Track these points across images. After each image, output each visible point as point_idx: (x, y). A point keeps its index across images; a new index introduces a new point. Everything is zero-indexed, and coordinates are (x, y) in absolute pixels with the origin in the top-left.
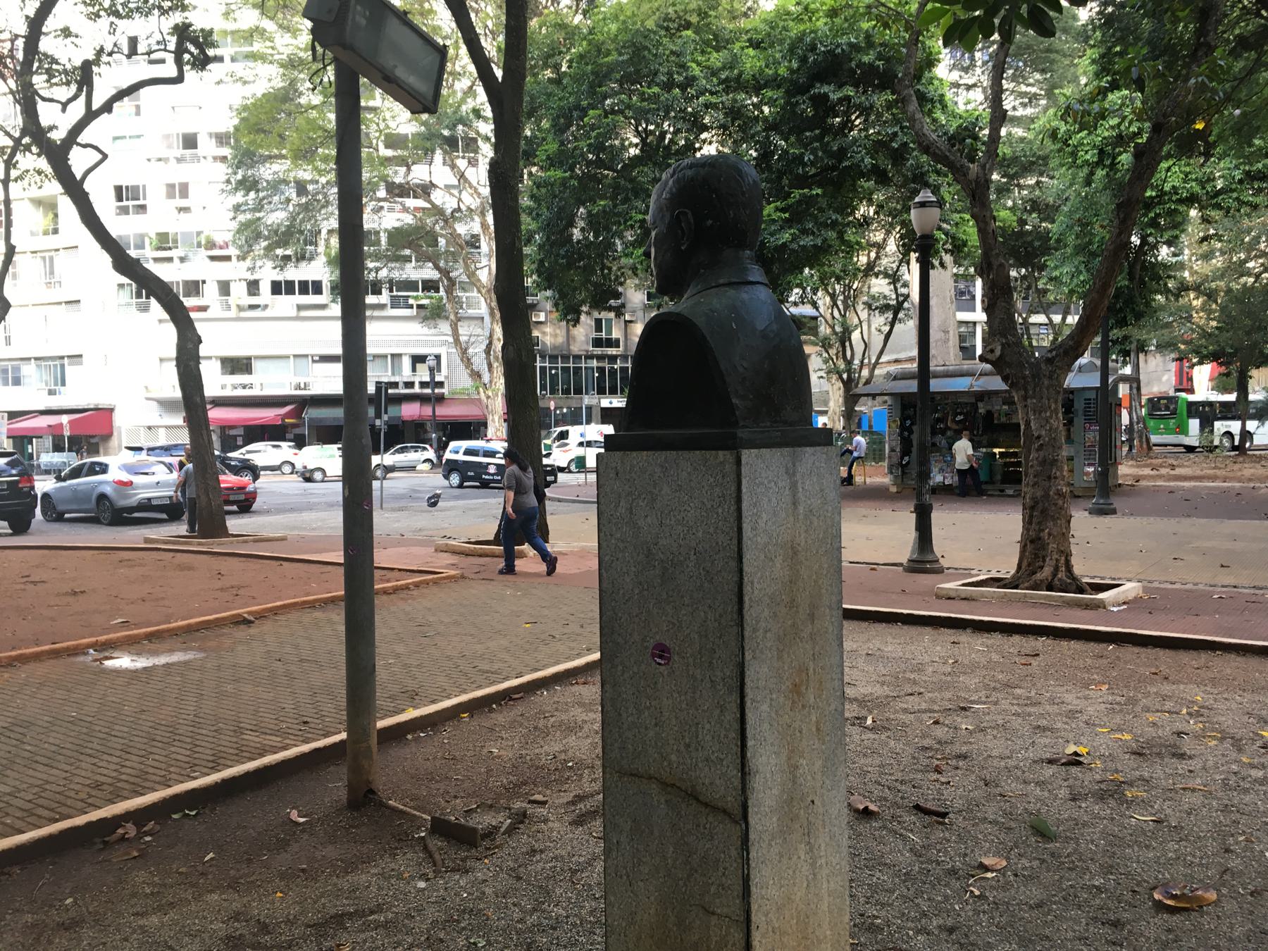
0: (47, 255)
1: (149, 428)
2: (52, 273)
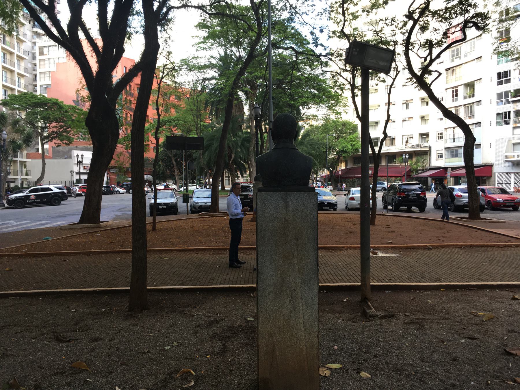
0: (469, 105)
1: (507, 173)
2: (471, 112)
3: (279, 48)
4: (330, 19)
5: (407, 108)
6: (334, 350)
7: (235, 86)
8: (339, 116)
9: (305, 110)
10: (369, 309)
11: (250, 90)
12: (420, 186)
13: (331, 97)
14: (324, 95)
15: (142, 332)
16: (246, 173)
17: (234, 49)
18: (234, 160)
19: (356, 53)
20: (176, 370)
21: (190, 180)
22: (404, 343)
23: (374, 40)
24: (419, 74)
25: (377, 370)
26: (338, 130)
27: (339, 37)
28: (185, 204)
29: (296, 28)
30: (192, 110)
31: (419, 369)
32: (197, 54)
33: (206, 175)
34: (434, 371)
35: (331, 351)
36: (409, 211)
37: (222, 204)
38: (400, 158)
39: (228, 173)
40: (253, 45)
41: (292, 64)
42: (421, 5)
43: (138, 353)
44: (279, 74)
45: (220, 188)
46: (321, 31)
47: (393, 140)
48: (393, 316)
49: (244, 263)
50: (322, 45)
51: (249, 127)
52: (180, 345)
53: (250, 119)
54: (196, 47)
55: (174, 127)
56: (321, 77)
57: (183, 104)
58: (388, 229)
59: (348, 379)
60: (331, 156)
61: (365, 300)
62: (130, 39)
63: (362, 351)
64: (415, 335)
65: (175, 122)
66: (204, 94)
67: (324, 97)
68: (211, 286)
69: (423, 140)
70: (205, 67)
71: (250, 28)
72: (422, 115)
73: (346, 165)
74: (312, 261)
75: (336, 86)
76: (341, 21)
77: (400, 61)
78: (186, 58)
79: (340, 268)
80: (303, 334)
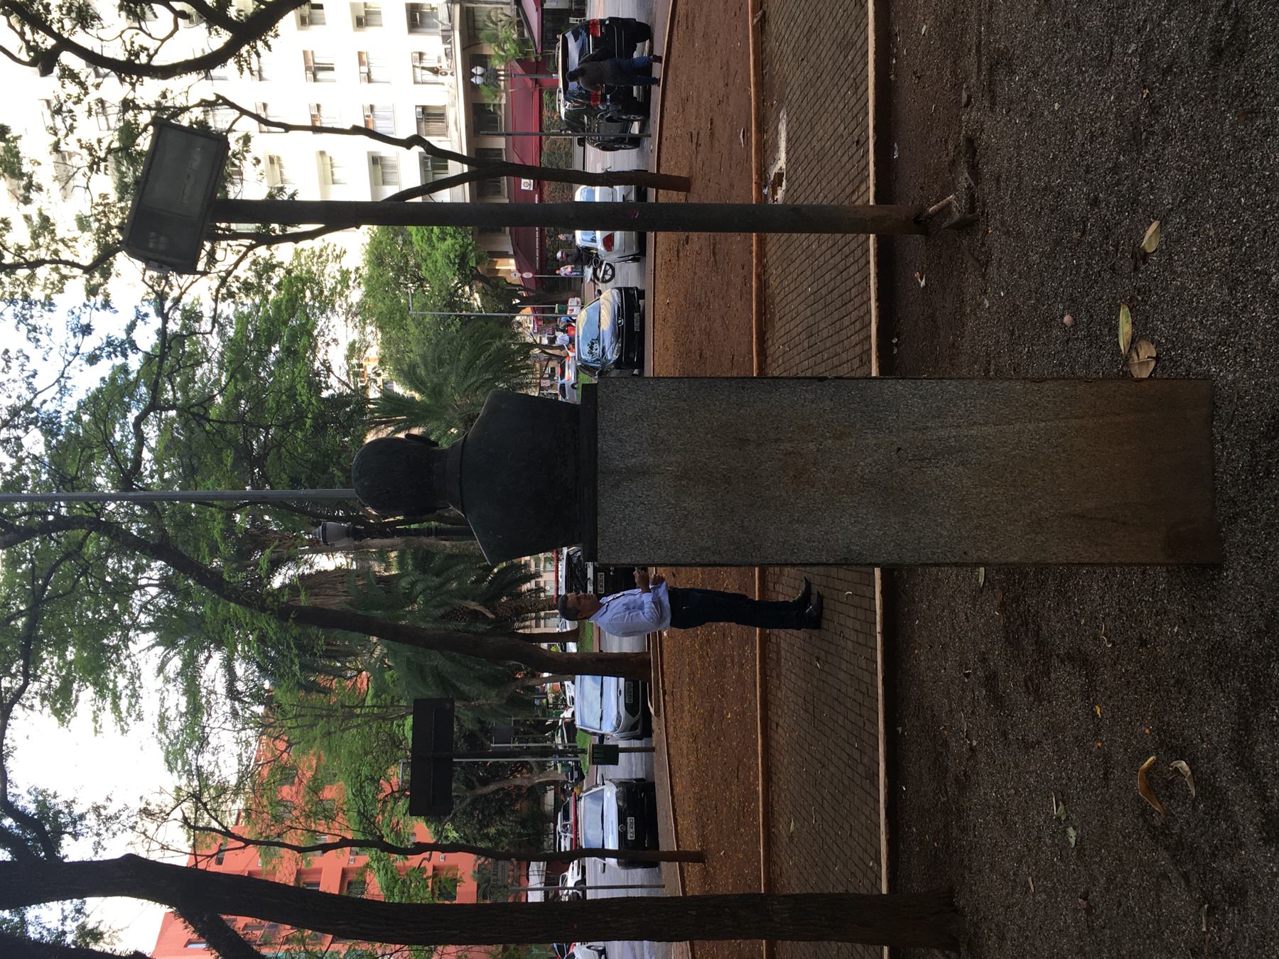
3: (138, 461)
4: (48, 304)
5: (332, 69)
6: (1075, 324)
7: (255, 598)
8: (353, 276)
9: (332, 381)
10: (950, 212)
11: (268, 551)
12: (570, 36)
13: (292, 302)
14: (286, 322)
15: (1023, 914)
16: (527, 565)
17: (137, 599)
18: (484, 604)
19: (163, 239)
20: (1142, 815)
21: (547, 739)
22: (1053, 112)
23: (119, 171)
24: (226, 36)
25: (1135, 201)
26: (396, 279)
27: (106, 275)
28: (621, 755)
29: (74, 408)
30: (329, 733)
31: (1133, 75)
32: (151, 718)
33: (532, 689)
34: (1139, 31)
35: (1081, 334)
36: (646, 67)
37: (618, 645)
38: (485, 91)
39: (524, 620)
40: (124, 543)
41: (187, 421)
42: (10, 26)
43: (1091, 928)
44: (220, 461)
45: (572, 647)
46: (87, 330)
47: (428, 115)
48: (970, 141)
49: (808, 584)
50: (131, 327)
51: (382, 557)
52: (1064, 799)
53: (360, 554)
54: (130, 720)
55: (379, 789)
56: (231, 332)
57: (308, 765)
58: (704, 139)
59: (1165, 289)
60: (477, 301)
61: (921, 223)
62: (101, 934)
63: (1079, 243)
64: (1029, 79)
65: (365, 784)
66: (278, 694)
67: (293, 322)
68: (880, 691)
69: (427, 21)
70: (192, 690)
71: (74, 552)
72: (349, 22)
73: (505, 255)
74: (809, 396)
75: (260, 285)
76: (57, 270)
77: (187, 91)
78: (162, 754)
79: (824, 291)
80: (1030, 427)
